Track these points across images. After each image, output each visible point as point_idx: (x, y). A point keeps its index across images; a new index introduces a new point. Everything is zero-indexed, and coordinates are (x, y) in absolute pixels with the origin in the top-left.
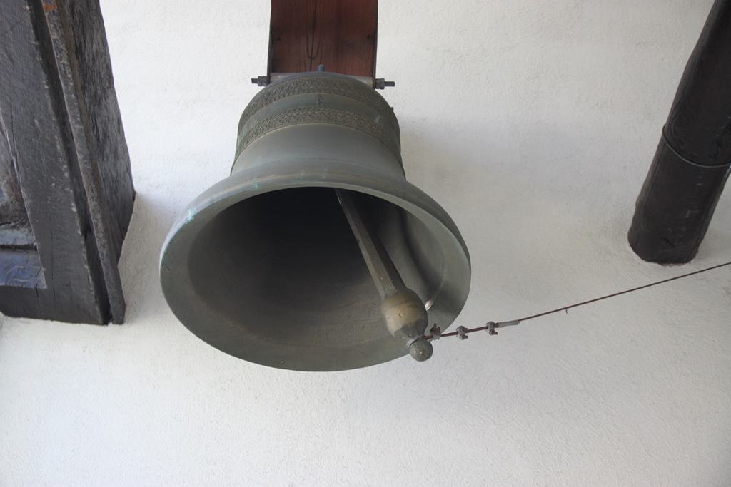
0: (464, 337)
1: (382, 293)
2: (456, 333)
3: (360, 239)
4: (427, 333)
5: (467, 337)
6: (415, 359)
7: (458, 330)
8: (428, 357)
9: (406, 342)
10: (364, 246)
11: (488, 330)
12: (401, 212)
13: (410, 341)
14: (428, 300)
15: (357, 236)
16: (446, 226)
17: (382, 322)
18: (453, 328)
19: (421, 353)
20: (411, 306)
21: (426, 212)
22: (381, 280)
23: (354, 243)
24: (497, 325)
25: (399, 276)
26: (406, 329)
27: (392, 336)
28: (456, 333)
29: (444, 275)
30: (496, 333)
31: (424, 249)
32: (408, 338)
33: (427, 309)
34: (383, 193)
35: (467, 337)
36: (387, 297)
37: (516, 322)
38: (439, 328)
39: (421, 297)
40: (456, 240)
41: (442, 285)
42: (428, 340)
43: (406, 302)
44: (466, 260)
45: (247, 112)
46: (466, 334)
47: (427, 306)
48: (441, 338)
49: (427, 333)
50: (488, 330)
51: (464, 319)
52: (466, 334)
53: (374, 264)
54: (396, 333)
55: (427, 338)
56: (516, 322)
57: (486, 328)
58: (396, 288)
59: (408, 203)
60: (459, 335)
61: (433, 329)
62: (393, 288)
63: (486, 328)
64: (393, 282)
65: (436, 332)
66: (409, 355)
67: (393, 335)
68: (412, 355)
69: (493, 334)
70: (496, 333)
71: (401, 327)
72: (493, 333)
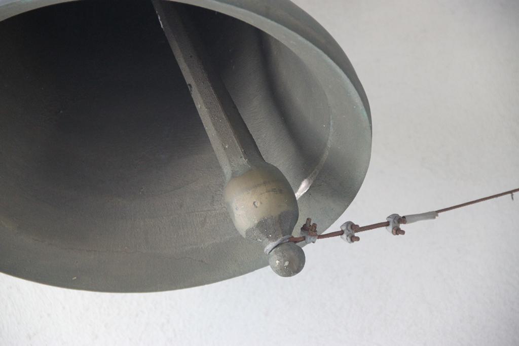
0: (353, 239)
1: (227, 170)
2: (341, 233)
3: (193, 84)
4: (296, 233)
5: (358, 239)
6: (277, 272)
7: (344, 228)
8: (298, 270)
9: (263, 247)
10: (199, 95)
11: (390, 228)
12: (260, 37)
13: (270, 246)
14: (305, 178)
15: (189, 79)
16: (338, 64)
17: (227, 217)
18: (336, 227)
19: (287, 263)
20: (274, 190)
21: (300, 38)
22: (225, 149)
23: (184, 89)
24: (403, 220)
25: (256, 146)
26: (262, 226)
27: (263, 249)
28: (341, 233)
29: (330, 138)
30: (403, 232)
31: (298, 97)
32: (267, 240)
33: (297, 199)
34: (233, 7)
35: (358, 239)
36: (234, 176)
37: (433, 215)
38: (315, 225)
39: (289, 178)
40: (348, 81)
41: (327, 153)
42: (297, 244)
43: (265, 183)
44: (365, 113)
45: (216, 13)
46: (356, 235)
47: (302, 190)
48: (319, 241)
49: (296, 233)
50: (390, 228)
51: (356, 212)
52: (356, 235)
53: (214, 125)
54: (247, 232)
55: (296, 241)
56: (433, 215)
57: (387, 224)
58: (250, 161)
59: (310, 45)
60: (344, 236)
61: (305, 225)
62: (243, 161)
63: (387, 224)
64: (245, 153)
65: (311, 231)
66: (269, 267)
67: (244, 234)
68: (273, 267)
69: (397, 234)
70: (403, 232)
71: (256, 222)
72: (398, 231)
